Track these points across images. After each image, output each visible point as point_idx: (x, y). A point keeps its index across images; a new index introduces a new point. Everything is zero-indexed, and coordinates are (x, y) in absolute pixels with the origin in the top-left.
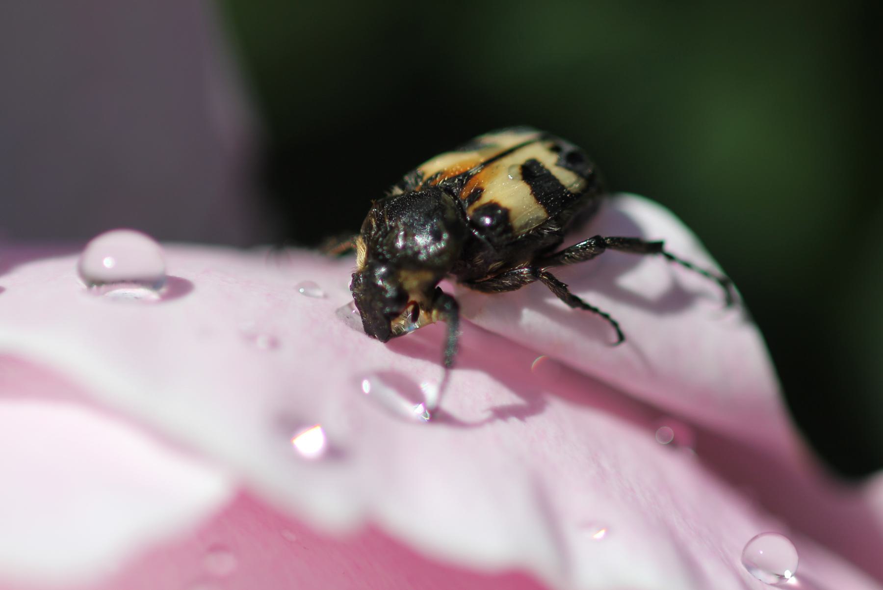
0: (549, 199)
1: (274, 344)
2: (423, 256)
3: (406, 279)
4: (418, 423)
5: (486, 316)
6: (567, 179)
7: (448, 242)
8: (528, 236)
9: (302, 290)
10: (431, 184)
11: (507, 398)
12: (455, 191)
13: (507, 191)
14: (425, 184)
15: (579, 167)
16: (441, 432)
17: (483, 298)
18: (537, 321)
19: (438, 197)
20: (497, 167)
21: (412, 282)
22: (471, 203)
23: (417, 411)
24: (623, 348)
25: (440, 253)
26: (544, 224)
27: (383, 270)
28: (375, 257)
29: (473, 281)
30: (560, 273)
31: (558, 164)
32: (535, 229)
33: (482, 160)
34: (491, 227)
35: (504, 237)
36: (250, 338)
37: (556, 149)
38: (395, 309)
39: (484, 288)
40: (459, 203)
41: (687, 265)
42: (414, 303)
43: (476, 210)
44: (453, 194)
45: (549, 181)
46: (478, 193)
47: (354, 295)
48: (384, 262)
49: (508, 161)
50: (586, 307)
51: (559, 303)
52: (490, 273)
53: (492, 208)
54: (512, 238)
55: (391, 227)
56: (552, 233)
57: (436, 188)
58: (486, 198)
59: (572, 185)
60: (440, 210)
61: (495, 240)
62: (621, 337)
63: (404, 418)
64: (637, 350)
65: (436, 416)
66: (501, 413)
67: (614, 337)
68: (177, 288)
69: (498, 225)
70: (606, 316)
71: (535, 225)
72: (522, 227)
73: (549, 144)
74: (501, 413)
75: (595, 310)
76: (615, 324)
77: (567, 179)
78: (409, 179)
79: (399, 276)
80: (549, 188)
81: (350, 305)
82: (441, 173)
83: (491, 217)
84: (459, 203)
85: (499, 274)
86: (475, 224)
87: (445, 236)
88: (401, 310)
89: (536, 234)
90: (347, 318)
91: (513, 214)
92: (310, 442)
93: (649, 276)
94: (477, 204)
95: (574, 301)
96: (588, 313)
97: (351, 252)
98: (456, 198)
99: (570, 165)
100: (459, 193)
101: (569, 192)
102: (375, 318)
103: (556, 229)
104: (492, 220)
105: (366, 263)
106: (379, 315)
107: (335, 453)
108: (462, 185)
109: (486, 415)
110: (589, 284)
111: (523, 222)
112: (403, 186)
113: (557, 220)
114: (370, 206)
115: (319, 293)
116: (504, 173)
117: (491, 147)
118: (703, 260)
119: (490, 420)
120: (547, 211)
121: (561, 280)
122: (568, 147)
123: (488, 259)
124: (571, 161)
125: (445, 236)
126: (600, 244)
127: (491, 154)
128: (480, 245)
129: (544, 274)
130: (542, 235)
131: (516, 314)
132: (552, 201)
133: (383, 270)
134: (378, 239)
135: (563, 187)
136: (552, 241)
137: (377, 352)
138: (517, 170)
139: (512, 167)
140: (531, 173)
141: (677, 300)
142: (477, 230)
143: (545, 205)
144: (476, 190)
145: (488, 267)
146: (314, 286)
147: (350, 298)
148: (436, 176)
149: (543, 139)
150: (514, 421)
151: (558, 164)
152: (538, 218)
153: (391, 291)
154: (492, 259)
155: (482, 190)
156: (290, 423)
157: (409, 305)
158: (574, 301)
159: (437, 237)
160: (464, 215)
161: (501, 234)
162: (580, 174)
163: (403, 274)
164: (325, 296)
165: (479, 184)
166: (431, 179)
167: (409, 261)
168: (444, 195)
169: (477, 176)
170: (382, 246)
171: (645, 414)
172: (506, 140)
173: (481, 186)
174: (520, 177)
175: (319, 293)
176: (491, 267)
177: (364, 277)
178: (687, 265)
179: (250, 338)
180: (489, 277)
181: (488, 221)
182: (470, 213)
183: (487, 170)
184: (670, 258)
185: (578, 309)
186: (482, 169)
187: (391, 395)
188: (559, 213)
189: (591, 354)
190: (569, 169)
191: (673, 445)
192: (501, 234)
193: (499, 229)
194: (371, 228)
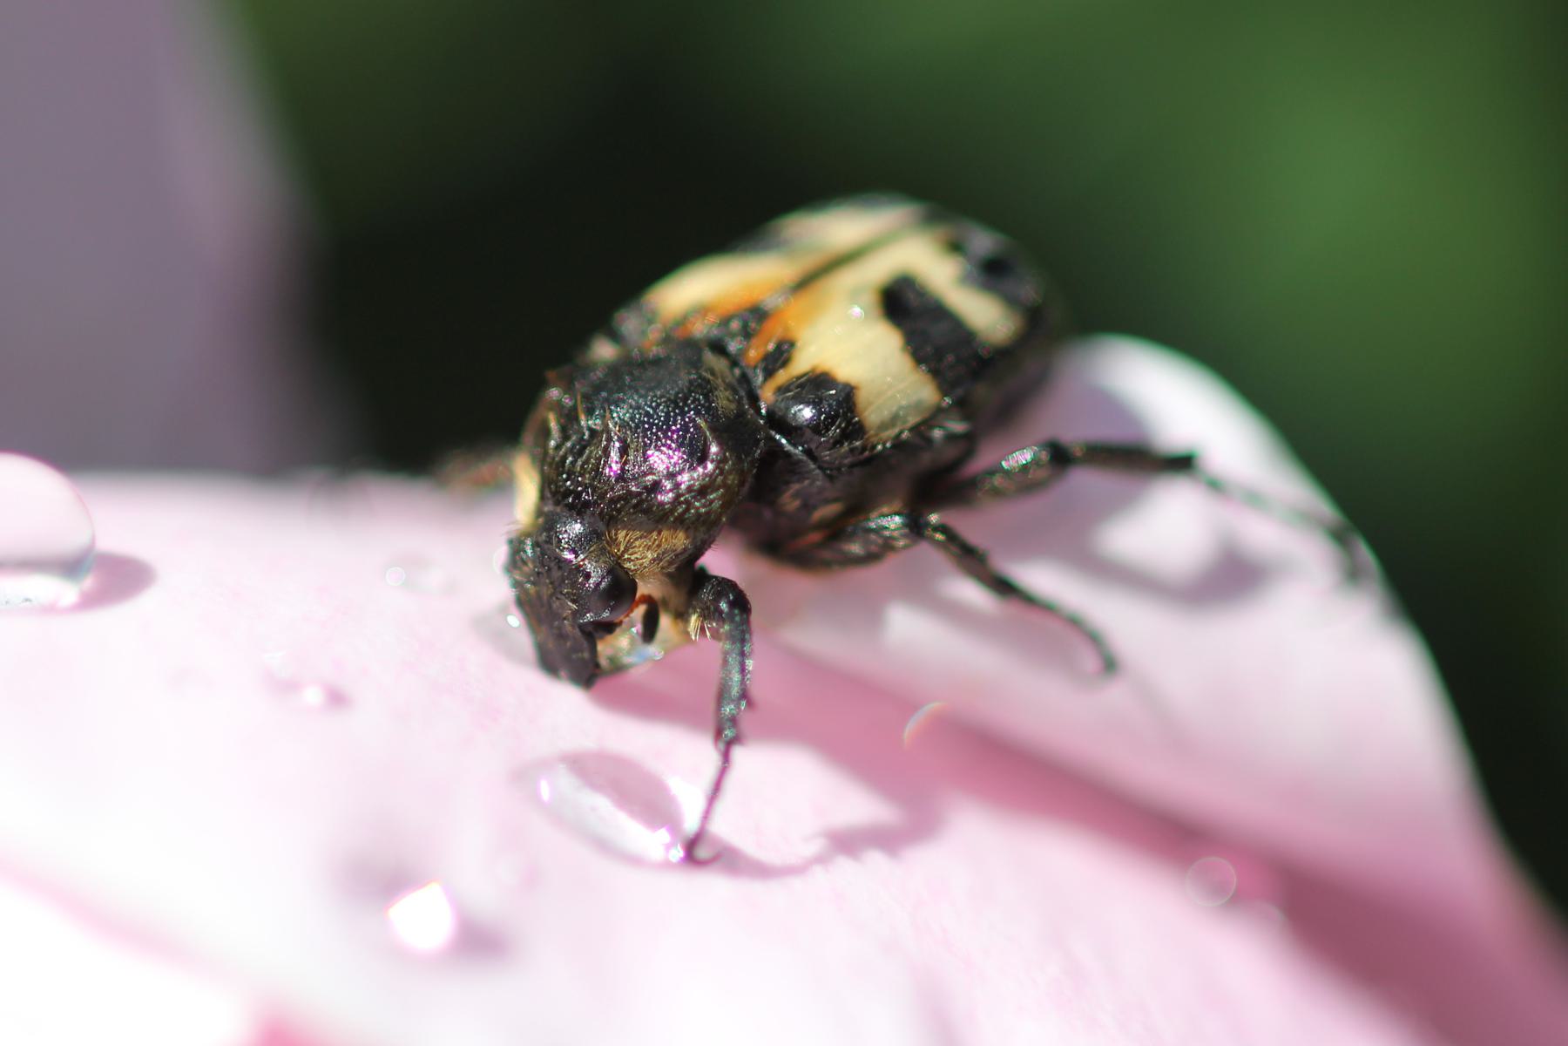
1: (337, 699)
5: (807, 626)
6: (985, 315)
7: (720, 463)
8: (898, 444)
11: (859, 806)
13: (850, 346)
16: (713, 886)
17: (796, 584)
18: (919, 631)
19: (696, 363)
21: (643, 553)
22: (769, 373)
23: (657, 844)
26: (934, 416)
27: (577, 528)
28: (560, 495)
29: (780, 545)
30: (971, 525)
32: (915, 429)
34: (816, 427)
37: (955, 247)
40: (745, 379)
42: (648, 600)
43: (782, 390)
46: (780, 355)
47: (517, 585)
48: (579, 509)
52: (822, 525)
53: (816, 384)
54: (864, 448)
55: (593, 432)
56: (951, 438)
58: (804, 361)
61: (826, 455)
62: (1110, 665)
63: (635, 860)
65: (698, 852)
66: (847, 843)
67: (1090, 661)
68: (116, 578)
69: (831, 420)
71: (913, 420)
72: (884, 426)
74: (847, 843)
77: (985, 315)
78: (629, 323)
79: (614, 541)
82: (702, 310)
83: (816, 404)
85: (836, 531)
86: (778, 421)
91: (862, 398)
92: (423, 919)
93: (1164, 527)
94: (782, 377)
95: (1003, 587)
96: (1034, 617)
97: (504, 486)
98: (734, 363)
100: (743, 352)
102: (561, 636)
105: (539, 513)
106: (572, 623)
107: (478, 942)
108: (747, 334)
109: (814, 848)
111: (886, 414)
112: (615, 336)
113: (963, 406)
114: (543, 385)
116: (837, 300)
119: (821, 860)
122: (984, 241)
123: (809, 496)
125: (714, 449)
126: (1060, 457)
128: (793, 468)
130: (929, 441)
131: (873, 617)
133: (577, 528)
134: (564, 458)
136: (951, 453)
137: (567, 710)
138: (871, 299)
140: (901, 303)
141: (1231, 578)
143: (936, 373)
150: (875, 859)
153: (596, 573)
154: (811, 490)
155: (792, 344)
156: (379, 879)
157: (633, 603)
158: (1003, 587)
160: (754, 399)
161: (838, 442)
162: (1011, 301)
166: (683, 320)
167: (640, 507)
168: (710, 358)
171: (1168, 834)
172: (839, 227)
177: (536, 545)
179: (287, 687)
181: (807, 413)
182: (767, 396)
187: (601, 809)
191: (1236, 900)
192: (838, 442)
193: (834, 431)
194: (546, 433)
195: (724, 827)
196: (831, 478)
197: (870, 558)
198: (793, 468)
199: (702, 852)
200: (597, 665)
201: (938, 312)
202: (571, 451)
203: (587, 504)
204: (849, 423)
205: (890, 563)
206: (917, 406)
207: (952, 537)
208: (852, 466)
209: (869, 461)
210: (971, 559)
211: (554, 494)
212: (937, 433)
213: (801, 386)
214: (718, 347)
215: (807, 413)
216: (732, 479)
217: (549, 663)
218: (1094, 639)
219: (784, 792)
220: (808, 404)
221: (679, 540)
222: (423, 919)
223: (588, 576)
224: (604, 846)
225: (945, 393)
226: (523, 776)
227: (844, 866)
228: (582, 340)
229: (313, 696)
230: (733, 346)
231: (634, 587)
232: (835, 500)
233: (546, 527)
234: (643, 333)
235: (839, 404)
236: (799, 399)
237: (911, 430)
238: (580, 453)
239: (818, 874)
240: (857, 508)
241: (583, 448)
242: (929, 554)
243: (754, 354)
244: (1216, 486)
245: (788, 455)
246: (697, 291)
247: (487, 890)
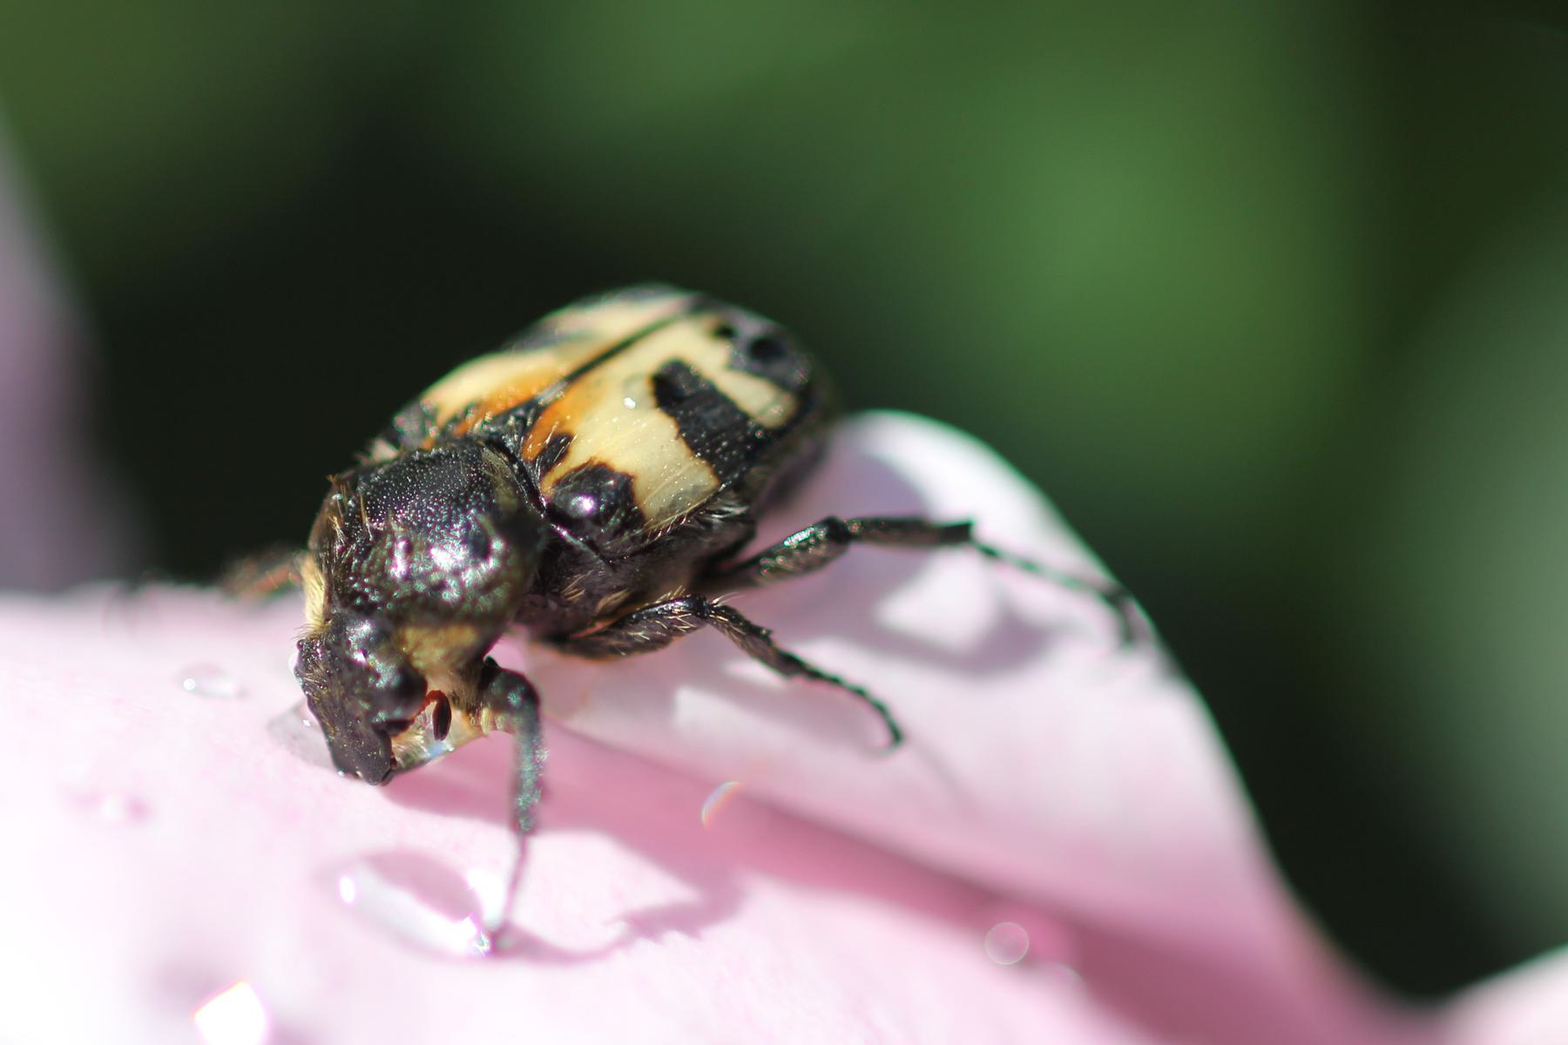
0: (718, 444)
1: (138, 810)
3: (418, 645)
4: (470, 959)
5: (596, 712)
6: (757, 398)
7: (504, 558)
8: (679, 531)
9: (189, 684)
10: (457, 431)
11: (658, 888)
12: (510, 443)
13: (625, 435)
14: (444, 432)
15: (779, 368)
16: (518, 976)
17: (584, 672)
18: (707, 712)
19: (475, 460)
21: (432, 651)
22: (547, 468)
23: (462, 936)
24: (903, 760)
25: (487, 587)
27: (365, 628)
28: (346, 599)
29: (563, 636)
34: (597, 519)
35: (626, 536)
36: (86, 801)
37: (724, 333)
38: (398, 713)
39: (590, 649)
40: (522, 469)
41: (1029, 566)
42: (438, 696)
43: (559, 483)
44: (506, 451)
45: (715, 406)
46: (559, 446)
47: (305, 688)
48: (367, 611)
49: (619, 369)
50: (815, 675)
51: (757, 672)
52: (602, 616)
53: (594, 476)
54: (644, 537)
55: (377, 533)
56: (730, 521)
57: (467, 440)
58: (579, 455)
59: (762, 412)
61: (608, 545)
62: (897, 735)
63: (436, 955)
64: (934, 762)
65: (504, 943)
66: (646, 925)
67: (880, 735)
69: (611, 510)
70: (860, 693)
72: (663, 514)
73: (709, 321)
74: (646, 925)
75: (835, 681)
76: (880, 709)
78: (406, 422)
79: (402, 641)
80: (715, 421)
81: (297, 710)
82: (477, 406)
83: (595, 495)
84: (522, 469)
85: (620, 618)
87: (497, 545)
89: (696, 525)
90: (294, 740)
91: (640, 487)
93: (945, 597)
94: (560, 470)
95: (789, 664)
96: (820, 689)
97: (289, 590)
98: (512, 459)
99: (757, 365)
101: (759, 427)
103: (738, 511)
104: (599, 503)
105: (327, 616)
106: (366, 726)
108: (524, 430)
109: (616, 931)
110: (817, 623)
111: (664, 502)
112: (394, 439)
113: (739, 489)
114: (326, 489)
115: (227, 687)
116: (611, 391)
117: (580, 338)
119: (622, 943)
120: (715, 472)
121: (756, 620)
122: (751, 326)
123: (593, 586)
124: (761, 355)
125: (497, 545)
126: (838, 534)
127: (582, 355)
128: (575, 560)
129: (718, 611)
130: (709, 525)
131: (663, 701)
132: (725, 451)
133: (365, 628)
134: (350, 561)
135: (746, 417)
136: (730, 536)
138: (643, 388)
139: (629, 381)
140: (673, 390)
141: (1012, 644)
142: (564, 526)
143: (710, 458)
144: (556, 440)
145: (595, 603)
146: (212, 671)
148: (466, 412)
149: (697, 309)
151: (732, 366)
152: (696, 488)
153: (386, 675)
154: (598, 579)
155: (569, 438)
158: (789, 664)
159: (480, 550)
160: (534, 494)
161: (618, 532)
162: (781, 384)
163: (411, 634)
164: (242, 694)
165: (562, 423)
166: (455, 420)
167: (425, 606)
168: (497, 460)
169: (557, 407)
170: (358, 575)
172: (610, 319)
173: (567, 428)
175: (227, 687)
176: (601, 604)
177: (326, 647)
178: (1029, 566)
179: (86, 801)
180: (599, 626)
181: (586, 505)
182: (547, 489)
183: (578, 391)
184: (990, 553)
185: (799, 683)
186: (566, 390)
188: (742, 474)
189: (833, 777)
191: (1029, 962)
192: (618, 532)
193: (614, 521)
194: (332, 536)
195: (530, 918)
196: (613, 567)
197: (656, 643)
198: (575, 560)
199: (507, 942)
201: (713, 396)
202: (356, 554)
203: (374, 605)
204: (629, 511)
205: (677, 644)
207: (733, 617)
208: (633, 554)
209: (650, 548)
210: (755, 639)
211: (341, 596)
213: (580, 478)
214: (496, 444)
215: (586, 505)
216: (517, 574)
217: (343, 763)
219: (584, 878)
220: (587, 495)
221: (467, 637)
223: (378, 676)
224: (411, 944)
225: (721, 479)
226: (325, 877)
227: (645, 948)
228: (364, 447)
229: (111, 810)
232: (619, 589)
233: (335, 628)
234: (424, 433)
235: (618, 493)
236: (578, 491)
237: (690, 514)
238: (366, 555)
239: (620, 959)
240: (641, 594)
241: (368, 550)
242: (713, 636)
243: (532, 449)
244: (990, 553)
245: (570, 547)
246: (473, 388)
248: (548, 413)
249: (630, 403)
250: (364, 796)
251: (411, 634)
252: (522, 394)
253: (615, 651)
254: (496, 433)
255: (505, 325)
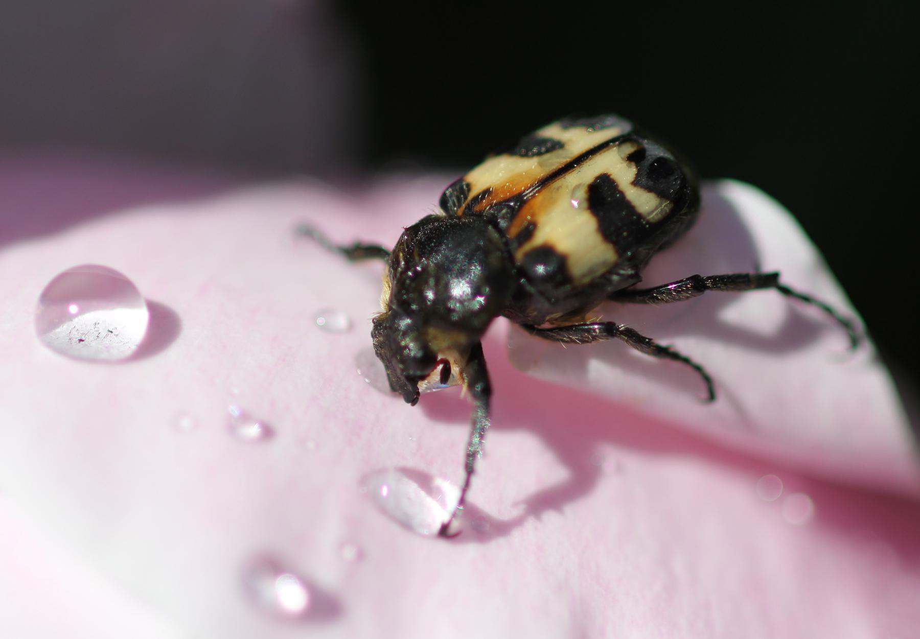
1: (268, 432)
2: (455, 317)
3: (435, 338)
13: (567, 228)
18: (606, 375)
19: (482, 233)
20: (558, 189)
26: (613, 269)
27: (408, 321)
31: (635, 183)
33: (542, 173)
34: (547, 278)
40: (507, 244)
41: (806, 299)
46: (529, 231)
48: (409, 313)
50: (675, 356)
53: (546, 253)
57: (480, 215)
58: (541, 238)
60: (482, 254)
72: (584, 276)
75: (686, 361)
76: (698, 369)
77: (646, 203)
86: (523, 272)
88: (426, 373)
93: (758, 310)
94: (528, 247)
96: (677, 365)
99: (651, 183)
101: (648, 222)
105: (390, 307)
116: (562, 188)
117: (557, 146)
118: (830, 294)
122: (655, 151)
127: (556, 160)
130: (610, 281)
131: (581, 366)
133: (408, 321)
135: (640, 216)
138: (582, 194)
139: (577, 187)
141: (795, 335)
144: (527, 228)
147: (370, 342)
151: (635, 183)
156: (271, 565)
157: (438, 363)
160: (511, 258)
163: (432, 331)
165: (533, 215)
166: (476, 199)
167: (438, 315)
172: (578, 139)
174: (585, 205)
182: (519, 255)
183: (545, 192)
184: (786, 291)
190: (649, 189)
200: (418, 393)
203: (413, 311)
206: (604, 263)
212: (615, 278)
215: (541, 269)
218: (708, 380)
220: (541, 263)
221: (462, 339)
222: (290, 595)
226: (368, 479)
230: (503, 223)
231: (436, 358)
239: (531, 533)
243: (514, 231)
244: (786, 291)
247: (328, 575)
248: (527, 207)
249: (575, 203)
250: (401, 405)
251: (432, 331)
252: (516, 190)
253: (558, 340)
254: (493, 214)
255: (512, 142)
